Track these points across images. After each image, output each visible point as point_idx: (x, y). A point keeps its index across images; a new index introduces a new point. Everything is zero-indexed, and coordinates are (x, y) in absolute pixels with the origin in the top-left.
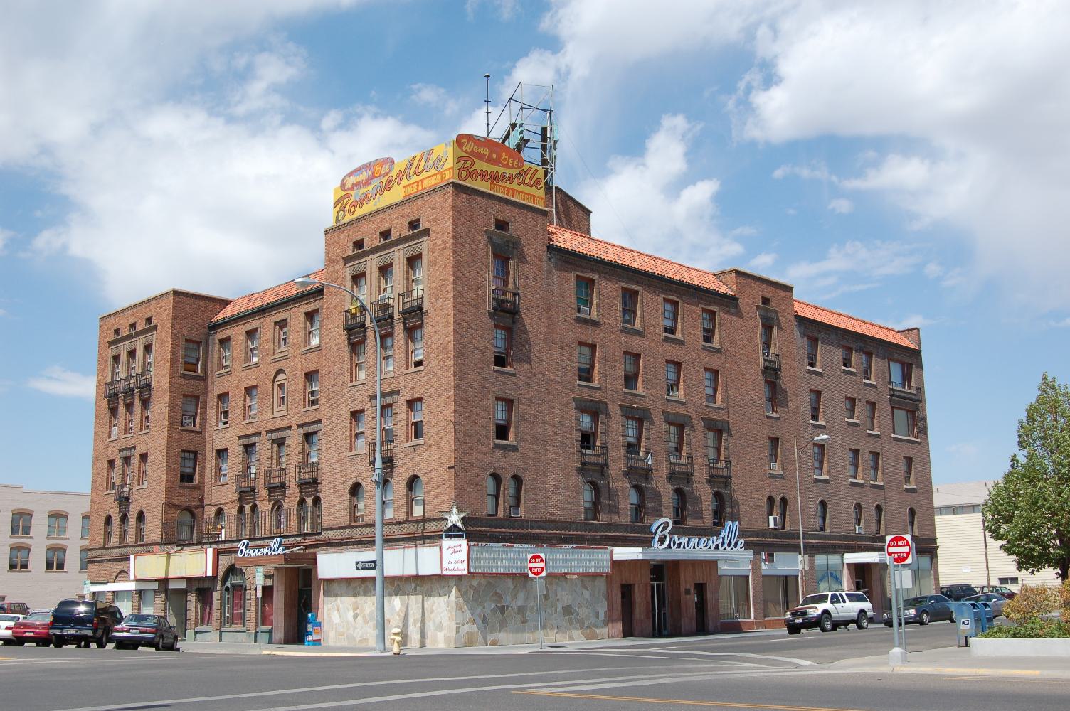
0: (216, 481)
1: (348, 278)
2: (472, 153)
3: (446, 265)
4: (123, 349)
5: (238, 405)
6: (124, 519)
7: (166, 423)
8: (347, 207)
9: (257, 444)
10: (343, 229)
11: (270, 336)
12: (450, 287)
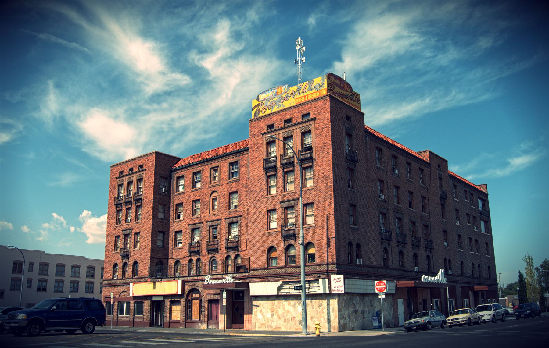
0: (175, 247)
1: (265, 143)
2: (334, 82)
3: (326, 136)
4: (125, 180)
5: (188, 209)
6: (125, 264)
7: (151, 217)
8: (261, 109)
9: (200, 228)
10: (261, 119)
11: (208, 175)
12: (330, 147)
